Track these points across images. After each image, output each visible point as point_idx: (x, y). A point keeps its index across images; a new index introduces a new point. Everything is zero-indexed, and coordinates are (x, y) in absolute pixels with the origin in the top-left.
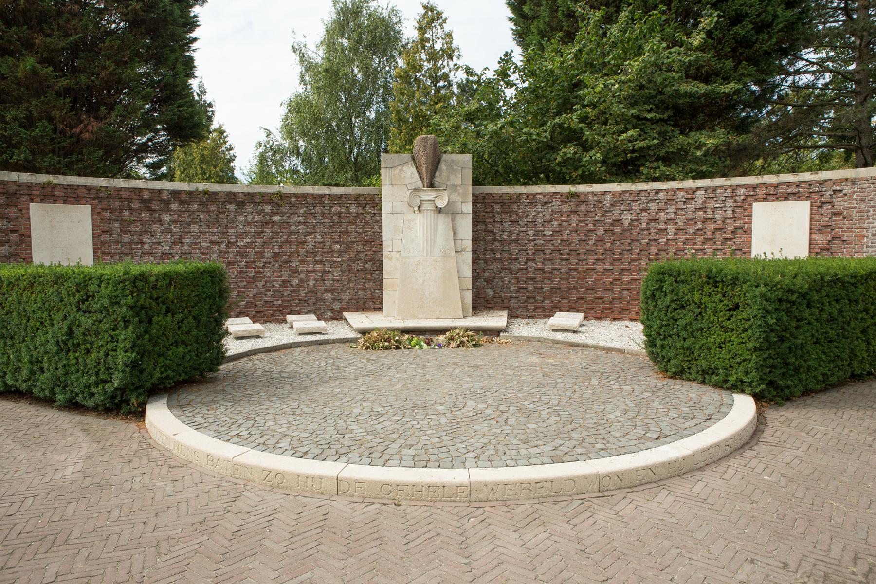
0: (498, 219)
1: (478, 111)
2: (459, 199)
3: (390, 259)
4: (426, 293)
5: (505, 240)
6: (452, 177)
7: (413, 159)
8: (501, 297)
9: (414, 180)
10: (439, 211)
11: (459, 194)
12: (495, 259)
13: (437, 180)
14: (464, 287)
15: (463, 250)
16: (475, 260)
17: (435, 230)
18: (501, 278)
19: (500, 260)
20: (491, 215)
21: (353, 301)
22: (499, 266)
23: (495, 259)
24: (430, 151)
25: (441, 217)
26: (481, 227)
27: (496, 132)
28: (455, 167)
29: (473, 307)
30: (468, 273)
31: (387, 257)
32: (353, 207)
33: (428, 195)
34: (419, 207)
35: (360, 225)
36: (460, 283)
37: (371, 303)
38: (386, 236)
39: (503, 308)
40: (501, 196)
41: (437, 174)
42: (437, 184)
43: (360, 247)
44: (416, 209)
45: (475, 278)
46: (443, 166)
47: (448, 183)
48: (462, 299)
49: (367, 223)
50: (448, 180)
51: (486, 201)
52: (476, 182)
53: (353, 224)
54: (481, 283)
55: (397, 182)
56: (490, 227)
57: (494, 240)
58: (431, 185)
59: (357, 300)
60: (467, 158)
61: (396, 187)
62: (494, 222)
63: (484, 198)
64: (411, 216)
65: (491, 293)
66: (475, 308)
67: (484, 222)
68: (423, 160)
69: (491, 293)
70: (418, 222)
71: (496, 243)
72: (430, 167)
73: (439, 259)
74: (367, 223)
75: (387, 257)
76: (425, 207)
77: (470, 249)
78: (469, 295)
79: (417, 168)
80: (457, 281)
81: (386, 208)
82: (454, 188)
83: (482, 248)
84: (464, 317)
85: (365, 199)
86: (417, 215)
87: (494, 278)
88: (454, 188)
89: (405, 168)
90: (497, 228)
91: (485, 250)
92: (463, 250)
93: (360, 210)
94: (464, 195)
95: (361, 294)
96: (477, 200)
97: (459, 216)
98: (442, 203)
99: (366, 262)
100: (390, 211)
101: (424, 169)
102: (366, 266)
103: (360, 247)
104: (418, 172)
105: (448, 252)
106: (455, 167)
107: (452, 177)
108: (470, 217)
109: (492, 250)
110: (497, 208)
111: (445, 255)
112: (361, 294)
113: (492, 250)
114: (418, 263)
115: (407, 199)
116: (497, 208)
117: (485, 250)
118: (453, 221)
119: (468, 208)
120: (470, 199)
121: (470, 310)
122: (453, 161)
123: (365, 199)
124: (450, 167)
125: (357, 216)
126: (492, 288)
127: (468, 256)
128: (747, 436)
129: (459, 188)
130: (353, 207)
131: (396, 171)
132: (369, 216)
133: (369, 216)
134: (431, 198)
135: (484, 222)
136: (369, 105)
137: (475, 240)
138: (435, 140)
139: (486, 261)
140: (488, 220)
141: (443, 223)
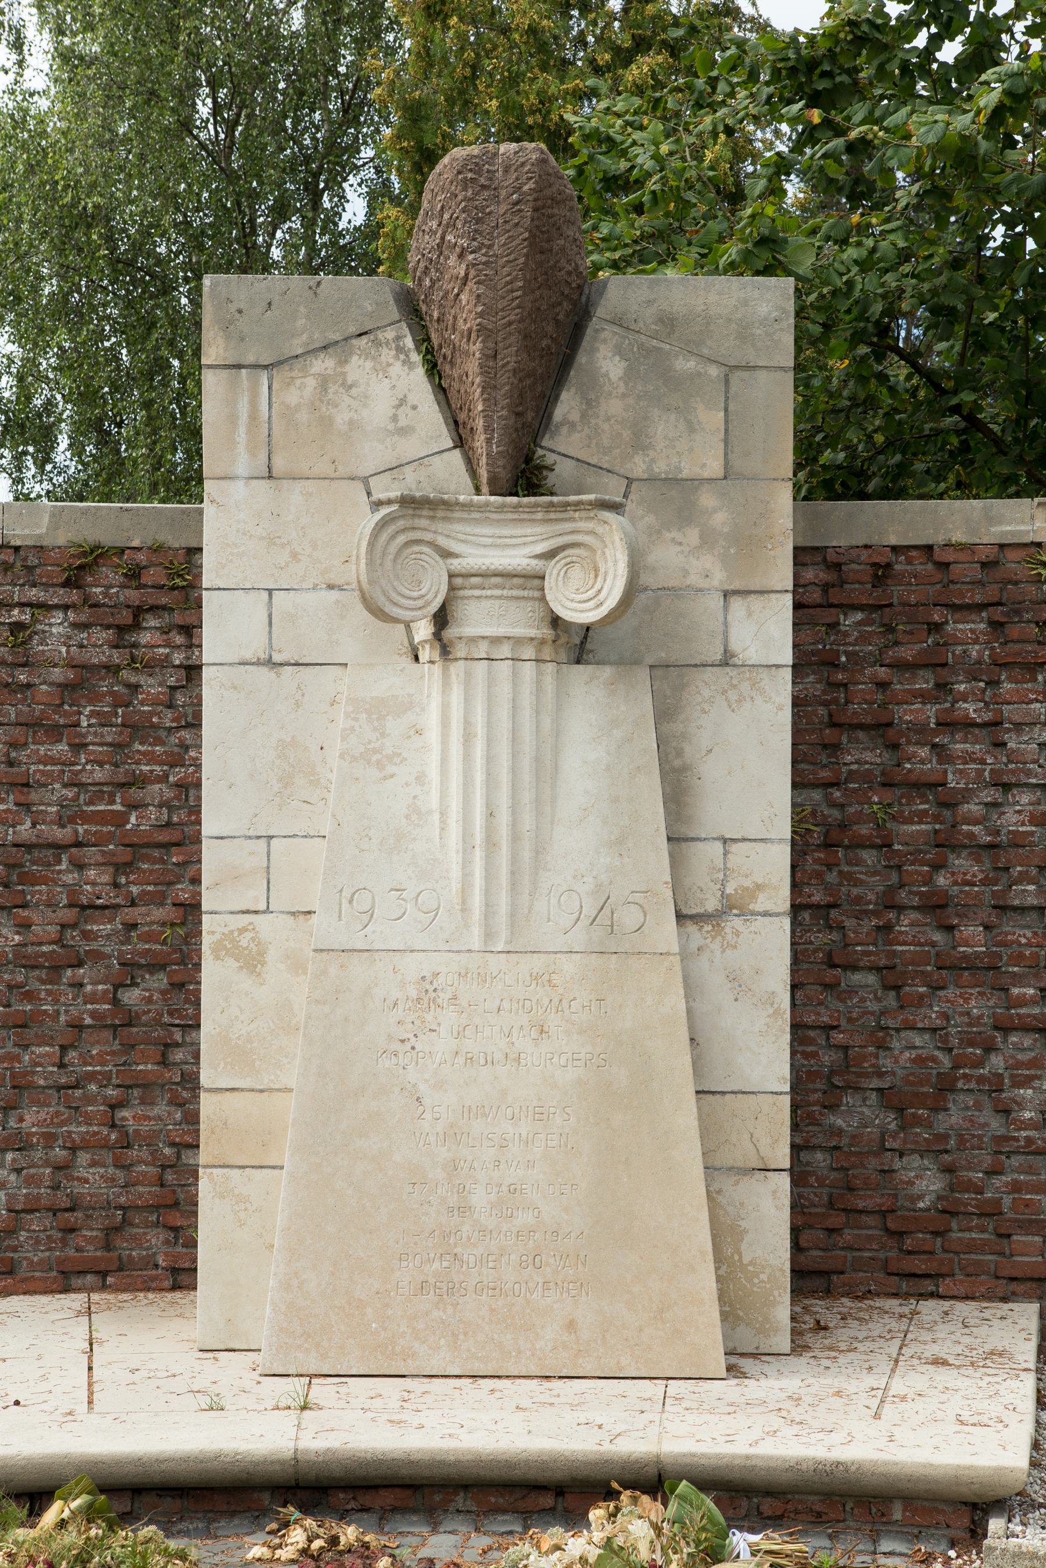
0: (970, 709)
1: (860, 41)
2: (708, 570)
3: (253, 962)
4: (479, 1198)
5: (1017, 841)
6: (663, 427)
7: (412, 310)
8: (991, 1211)
9: (411, 448)
10: (576, 645)
11: (707, 540)
12: (954, 967)
13: (565, 445)
14: (742, 1153)
15: (732, 906)
16: (816, 974)
17: (547, 772)
18: (995, 1085)
19: (986, 971)
20: (924, 682)
21: (36, 1223)
22: (981, 1006)
23: (954, 967)
24: (508, 246)
25: (588, 686)
26: (863, 755)
27: (962, 157)
28: (685, 365)
29: (798, 1273)
30: (764, 1059)
31: (230, 947)
32: (57, 625)
33: (501, 541)
34: (441, 619)
35: (99, 737)
36: (707, 1129)
37: (156, 1239)
38: (223, 813)
39: (1006, 1286)
40: (994, 560)
41: (567, 405)
42: (563, 470)
43: (96, 880)
44: (423, 630)
45: (817, 1087)
46: (605, 359)
47: (638, 467)
48: (725, 1236)
49: (138, 729)
50: (640, 443)
51: (896, 592)
52: (829, 473)
53: (55, 733)
54: (860, 1116)
55: (313, 455)
56: (921, 760)
57: (946, 843)
58: (523, 476)
59: (67, 1215)
60: (771, 300)
61: (295, 494)
62: (947, 724)
63: (881, 574)
64: (393, 677)
65: (926, 1184)
66: (811, 1278)
67: (882, 729)
68: (466, 312)
69: (926, 1184)
70: (432, 718)
71: (961, 862)
72: (510, 357)
73: (569, 966)
74: (138, 729)
75: (230, 947)
76: (480, 618)
77: (781, 897)
78: (769, 1212)
79: (433, 369)
80: (684, 1116)
81: (227, 629)
82: (676, 496)
83: (871, 890)
84: (739, 1361)
85: (134, 575)
86: (431, 672)
87: (946, 1086)
88: (676, 496)
89: (358, 368)
90: (967, 762)
91: (890, 904)
92: (732, 906)
93: (99, 647)
94: (744, 544)
95: (92, 1178)
96: (827, 591)
97: (706, 685)
98: (586, 595)
99: (130, 971)
100: (256, 648)
101: (469, 369)
102: (131, 997)
103: (96, 880)
104: (442, 391)
105: (629, 918)
106: (685, 365)
107: (663, 427)
108: (781, 690)
109: (936, 906)
110: (969, 634)
111: (609, 937)
112: (92, 1178)
113: (936, 906)
114: (427, 994)
115: (357, 570)
116: (969, 634)
117: (890, 904)
118: (665, 713)
119: (768, 633)
120: (781, 572)
121: (782, 1312)
122: (668, 322)
123: (134, 575)
124: (651, 366)
125: (81, 681)
126: (935, 1149)
127: (765, 949)
128: (441, 397)
129: (707, 499)
130: (57, 625)
131: (298, 390)
132: (152, 686)
133: (152, 686)
134: (517, 558)
135: (882, 729)
136: (337, 160)
137: (819, 844)
138: (546, 179)
139: (892, 977)
140: (907, 714)
141: (598, 725)
